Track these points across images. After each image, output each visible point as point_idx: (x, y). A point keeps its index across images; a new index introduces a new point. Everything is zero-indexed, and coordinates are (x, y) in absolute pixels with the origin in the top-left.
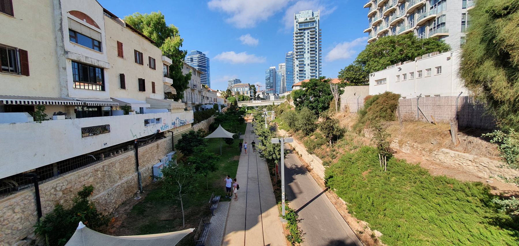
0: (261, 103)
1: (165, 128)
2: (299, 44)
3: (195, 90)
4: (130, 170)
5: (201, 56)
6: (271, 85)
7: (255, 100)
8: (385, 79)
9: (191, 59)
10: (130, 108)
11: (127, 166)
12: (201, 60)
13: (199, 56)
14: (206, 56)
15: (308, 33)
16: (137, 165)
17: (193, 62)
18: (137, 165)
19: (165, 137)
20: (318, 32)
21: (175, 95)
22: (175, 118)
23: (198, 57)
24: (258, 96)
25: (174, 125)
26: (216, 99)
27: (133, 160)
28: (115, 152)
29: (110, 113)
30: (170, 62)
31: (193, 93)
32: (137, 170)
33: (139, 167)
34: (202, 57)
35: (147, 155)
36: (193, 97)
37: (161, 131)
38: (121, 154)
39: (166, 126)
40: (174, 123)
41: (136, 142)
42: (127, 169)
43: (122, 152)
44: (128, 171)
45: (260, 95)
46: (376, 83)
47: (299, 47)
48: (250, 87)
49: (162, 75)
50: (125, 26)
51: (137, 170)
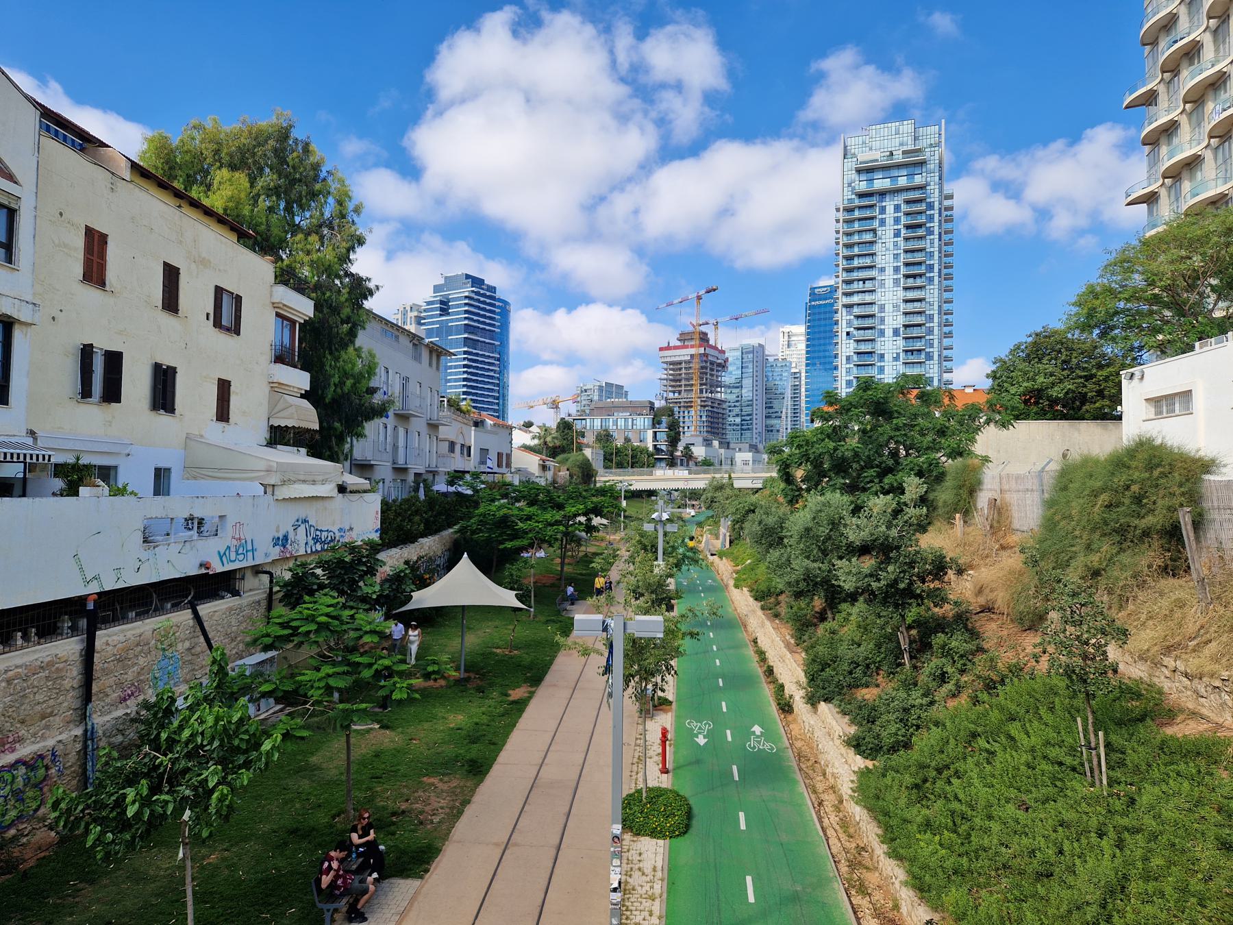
0: (686, 480)
1: (241, 557)
2: (856, 250)
3: (412, 419)
4: (51, 714)
5: (477, 293)
6: (747, 410)
7: (672, 463)
8: (1186, 395)
9: (442, 302)
10: (112, 473)
11: (39, 697)
12: (479, 308)
13: (473, 295)
14: (498, 295)
15: (897, 208)
16: (87, 693)
17: (448, 314)
18: (87, 693)
19: (236, 593)
20: (936, 205)
21: (308, 430)
22: (293, 521)
23: (466, 297)
24: (687, 448)
25: (284, 546)
26: (509, 456)
27: (74, 675)
28: (19, 634)
29: (18, 489)
30: (304, 307)
31: (401, 431)
32: (83, 716)
33: (95, 704)
34: (484, 295)
35: (142, 661)
36: (401, 443)
37: (218, 567)
38: (22, 648)
39: (244, 547)
40: (286, 538)
41: (90, 606)
42: (38, 708)
43: (26, 637)
44: (43, 717)
45: (692, 447)
46: (1153, 410)
47: (856, 263)
48: (655, 416)
49: (268, 354)
50: (126, 173)
51: (83, 716)
